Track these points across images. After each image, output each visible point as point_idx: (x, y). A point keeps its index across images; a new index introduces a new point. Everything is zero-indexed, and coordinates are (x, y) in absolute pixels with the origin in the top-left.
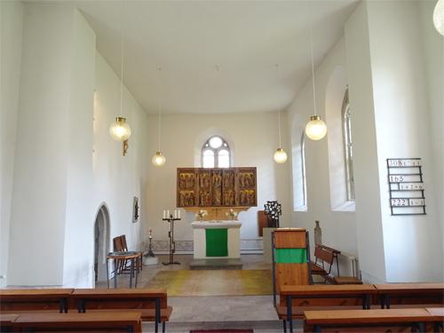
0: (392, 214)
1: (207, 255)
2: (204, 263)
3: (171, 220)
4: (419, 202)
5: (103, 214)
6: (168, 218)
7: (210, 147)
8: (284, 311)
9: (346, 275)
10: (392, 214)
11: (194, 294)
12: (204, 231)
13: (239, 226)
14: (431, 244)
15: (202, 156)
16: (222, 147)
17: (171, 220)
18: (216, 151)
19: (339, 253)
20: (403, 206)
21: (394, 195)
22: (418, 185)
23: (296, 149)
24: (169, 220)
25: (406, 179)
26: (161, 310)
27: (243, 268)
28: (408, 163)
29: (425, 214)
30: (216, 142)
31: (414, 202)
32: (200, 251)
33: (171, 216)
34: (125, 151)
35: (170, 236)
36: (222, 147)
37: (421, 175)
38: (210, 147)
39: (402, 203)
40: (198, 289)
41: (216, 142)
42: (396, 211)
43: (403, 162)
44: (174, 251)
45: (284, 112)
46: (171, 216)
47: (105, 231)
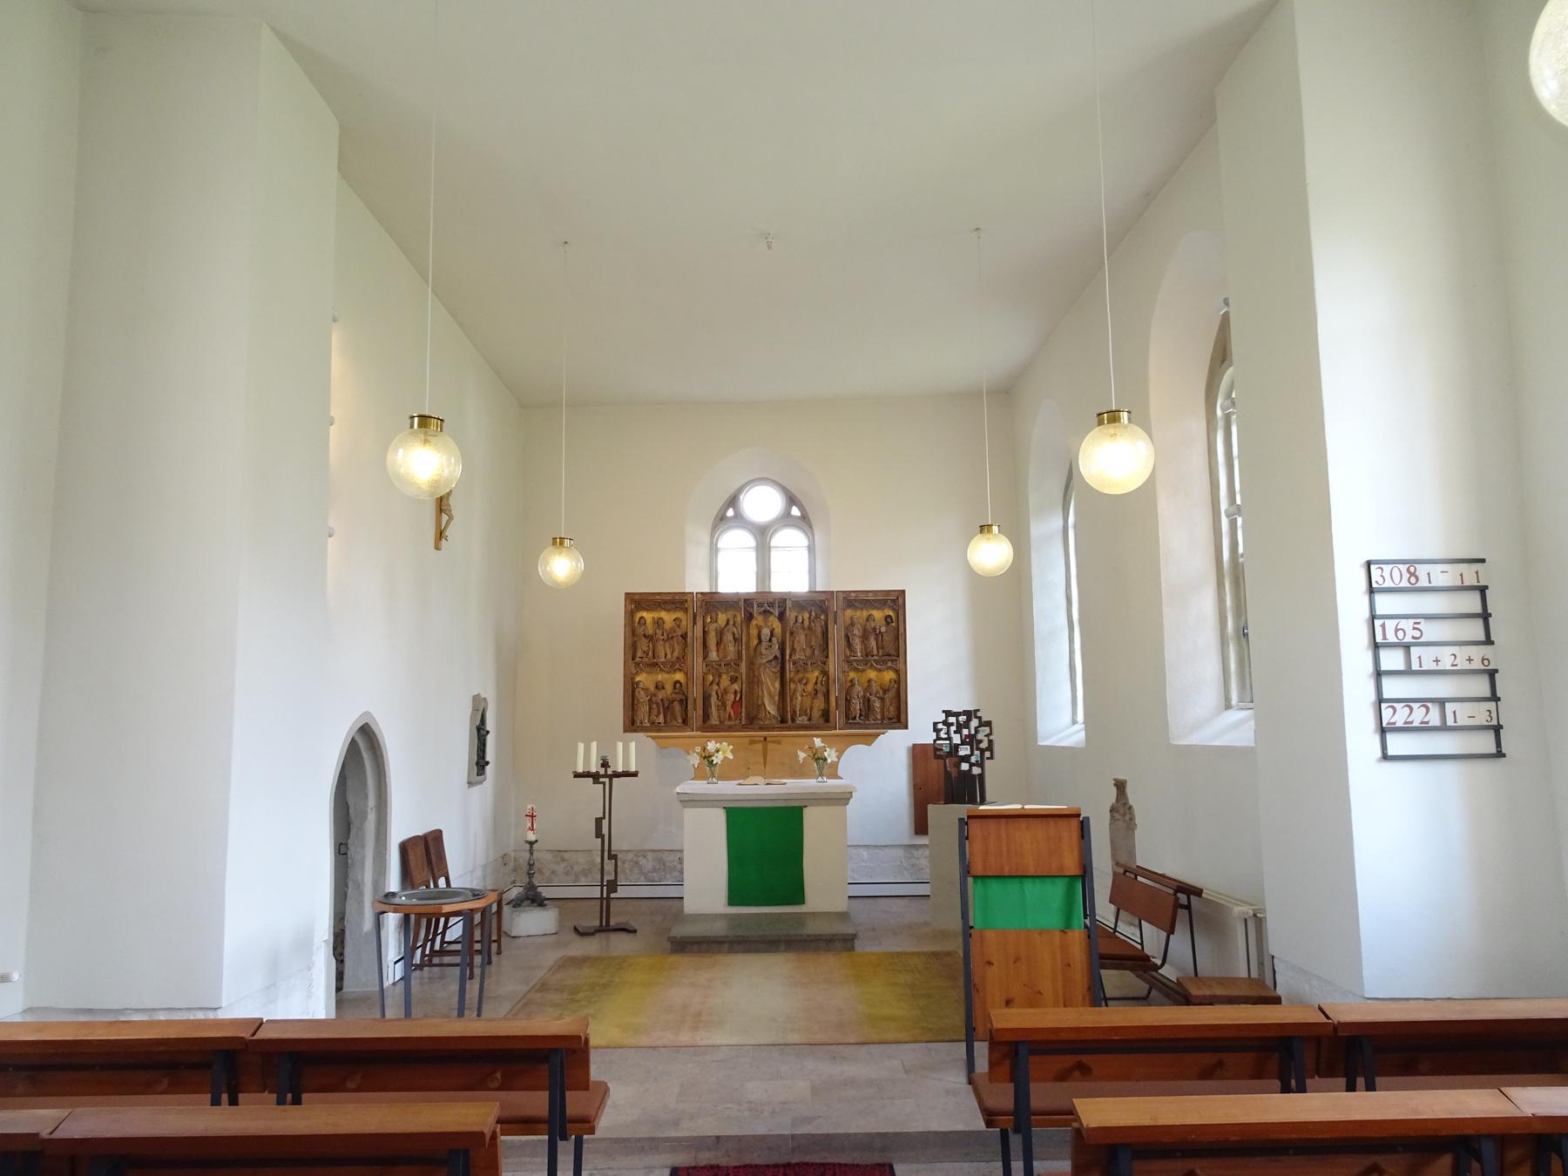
0: (1385, 757)
2: (719, 929)
7: (740, 521)
8: (1003, 1097)
10: (1385, 757)
13: (843, 798)
15: (714, 550)
16: (785, 520)
17: (604, 775)
18: (763, 534)
19: (1198, 892)
20: (1425, 728)
21: (1392, 688)
22: (1477, 652)
23: (1046, 527)
24: (596, 777)
29: (1500, 754)
30: (762, 503)
31: (1461, 714)
32: (705, 885)
33: (605, 765)
34: (440, 535)
35: (599, 834)
36: (785, 520)
37: (1485, 616)
38: (740, 521)
40: (699, 1020)
41: (762, 503)
42: (1397, 744)
43: (1422, 570)
45: (1005, 395)
46: (605, 765)
47: (372, 817)
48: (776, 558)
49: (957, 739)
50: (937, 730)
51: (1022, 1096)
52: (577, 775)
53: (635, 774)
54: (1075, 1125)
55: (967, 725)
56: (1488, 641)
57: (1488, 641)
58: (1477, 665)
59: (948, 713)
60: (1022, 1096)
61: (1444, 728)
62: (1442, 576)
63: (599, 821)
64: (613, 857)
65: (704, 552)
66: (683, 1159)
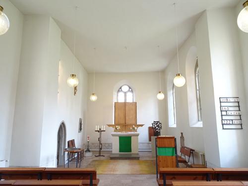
0: (223, 129)
1: (120, 151)
2: (118, 156)
3: (100, 131)
4: (238, 122)
5: (62, 129)
6: (98, 130)
10: (223, 129)
11: (112, 173)
12: (118, 138)
13: (138, 135)
14: (245, 146)
19: (194, 151)
20: (229, 124)
22: (238, 112)
24: (99, 131)
26: (93, 181)
27: (140, 159)
28: (232, 100)
32: (116, 149)
35: (99, 140)
42: (225, 127)
44: (101, 149)
47: (63, 137)
56: (239, 110)
57: (239, 110)
58: (238, 114)
61: (233, 124)
62: (232, 100)
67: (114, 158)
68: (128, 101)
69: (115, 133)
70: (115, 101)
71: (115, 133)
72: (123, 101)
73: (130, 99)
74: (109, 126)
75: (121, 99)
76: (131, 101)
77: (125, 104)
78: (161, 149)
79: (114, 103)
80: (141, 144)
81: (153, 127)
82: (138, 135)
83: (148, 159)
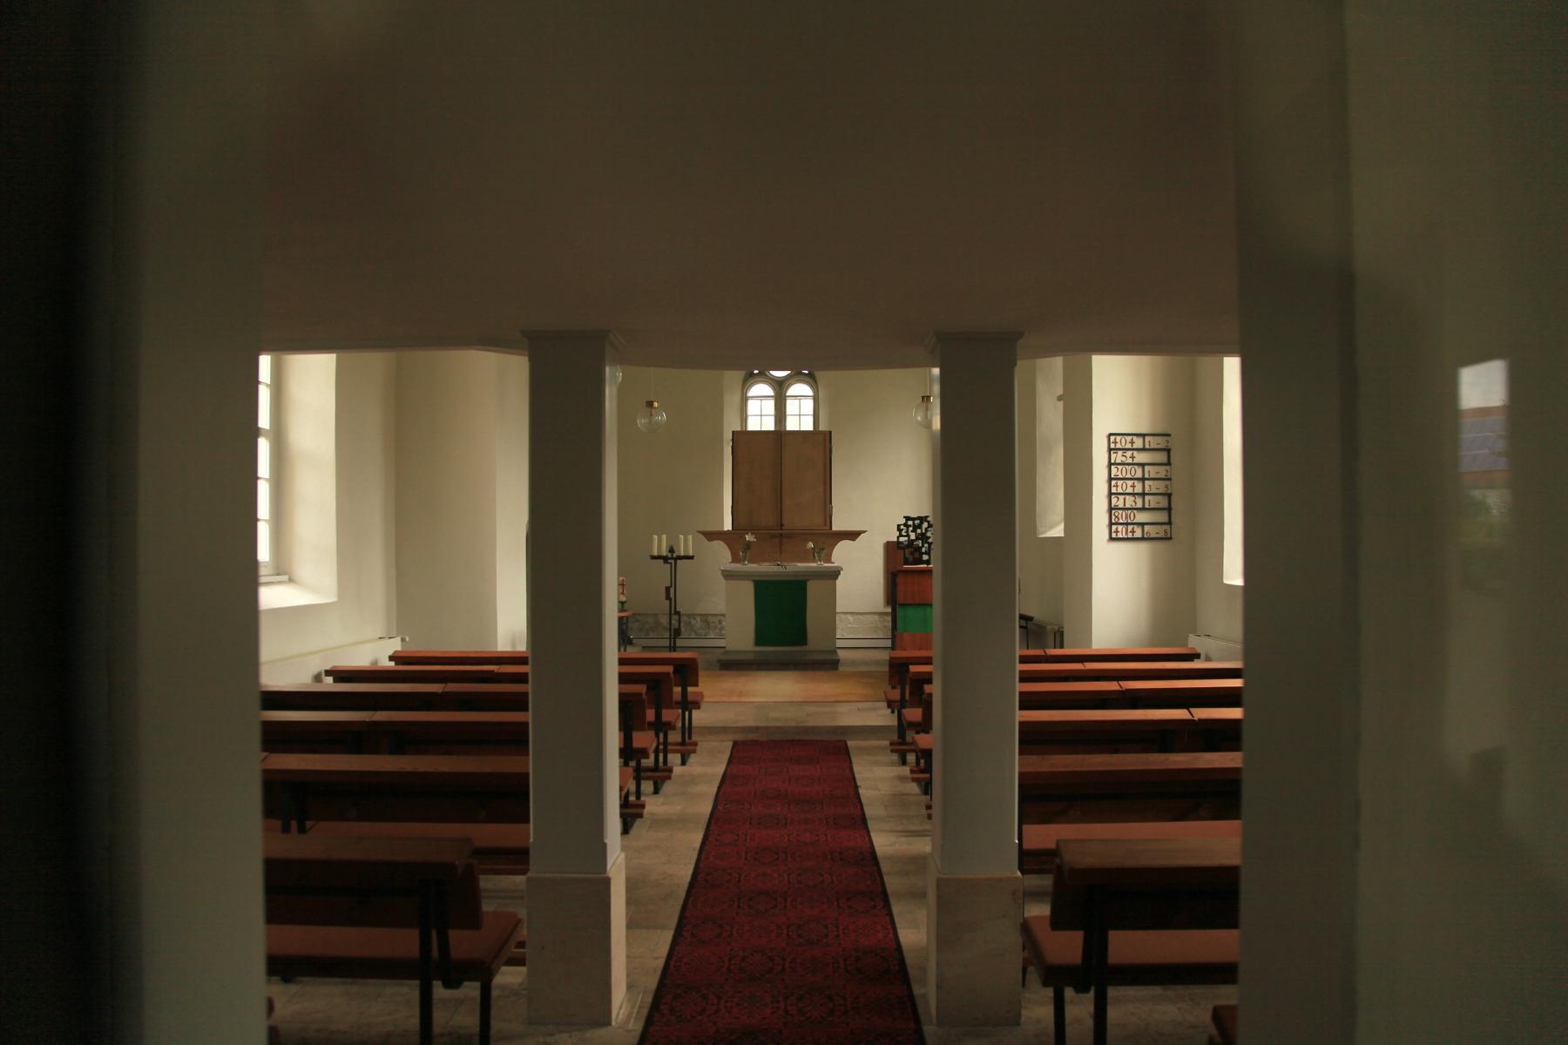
0: (1111, 539)
1: (760, 639)
2: (750, 657)
3: (672, 558)
4: (1163, 502)
6: (664, 553)
9: (1109, 1000)
10: (1111, 539)
11: (735, 699)
15: (744, 400)
17: (672, 558)
19: (1031, 619)
21: (1118, 502)
22: (1161, 484)
24: (665, 559)
25: (1141, 517)
27: (841, 669)
32: (739, 633)
33: (671, 551)
35: (668, 597)
37: (1169, 509)
39: (1130, 501)
40: (741, 694)
44: (677, 633)
46: (671, 551)
48: (791, 406)
49: (913, 536)
50: (899, 530)
51: (1095, 947)
52: (653, 558)
53: (691, 558)
54: (1058, 860)
55: (920, 526)
56: (1169, 464)
59: (908, 518)
60: (1095, 947)
63: (668, 589)
64: (678, 613)
65: (737, 398)
66: (739, 737)
67: (733, 664)
68: (792, 425)
69: (737, 567)
70: (731, 425)
71: (737, 567)
72: (769, 425)
73: (801, 414)
74: (712, 536)
75: (760, 416)
76: (807, 425)
77: (780, 436)
78: (911, 611)
79: (728, 436)
80: (850, 618)
81: (898, 542)
82: (835, 574)
83: (872, 668)
